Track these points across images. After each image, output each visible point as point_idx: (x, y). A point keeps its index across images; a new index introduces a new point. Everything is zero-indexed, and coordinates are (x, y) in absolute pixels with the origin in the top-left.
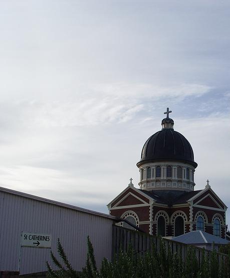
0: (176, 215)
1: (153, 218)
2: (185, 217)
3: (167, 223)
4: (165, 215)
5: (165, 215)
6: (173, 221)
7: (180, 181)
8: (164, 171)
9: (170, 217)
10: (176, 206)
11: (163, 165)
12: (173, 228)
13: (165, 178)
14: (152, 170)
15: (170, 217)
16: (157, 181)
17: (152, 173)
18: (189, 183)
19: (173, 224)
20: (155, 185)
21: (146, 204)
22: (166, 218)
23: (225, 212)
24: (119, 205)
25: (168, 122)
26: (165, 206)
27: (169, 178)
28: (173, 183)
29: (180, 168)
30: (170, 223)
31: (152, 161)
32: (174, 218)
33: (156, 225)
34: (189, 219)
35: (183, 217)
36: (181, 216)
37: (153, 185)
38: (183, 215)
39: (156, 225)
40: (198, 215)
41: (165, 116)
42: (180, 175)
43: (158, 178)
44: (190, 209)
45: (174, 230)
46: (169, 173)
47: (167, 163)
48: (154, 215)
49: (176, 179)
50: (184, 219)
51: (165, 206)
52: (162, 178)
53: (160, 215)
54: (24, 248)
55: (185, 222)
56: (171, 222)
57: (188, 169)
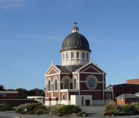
1: (61, 80)
16: (72, 60)
21: (58, 73)
29: (78, 54)
43: (72, 59)
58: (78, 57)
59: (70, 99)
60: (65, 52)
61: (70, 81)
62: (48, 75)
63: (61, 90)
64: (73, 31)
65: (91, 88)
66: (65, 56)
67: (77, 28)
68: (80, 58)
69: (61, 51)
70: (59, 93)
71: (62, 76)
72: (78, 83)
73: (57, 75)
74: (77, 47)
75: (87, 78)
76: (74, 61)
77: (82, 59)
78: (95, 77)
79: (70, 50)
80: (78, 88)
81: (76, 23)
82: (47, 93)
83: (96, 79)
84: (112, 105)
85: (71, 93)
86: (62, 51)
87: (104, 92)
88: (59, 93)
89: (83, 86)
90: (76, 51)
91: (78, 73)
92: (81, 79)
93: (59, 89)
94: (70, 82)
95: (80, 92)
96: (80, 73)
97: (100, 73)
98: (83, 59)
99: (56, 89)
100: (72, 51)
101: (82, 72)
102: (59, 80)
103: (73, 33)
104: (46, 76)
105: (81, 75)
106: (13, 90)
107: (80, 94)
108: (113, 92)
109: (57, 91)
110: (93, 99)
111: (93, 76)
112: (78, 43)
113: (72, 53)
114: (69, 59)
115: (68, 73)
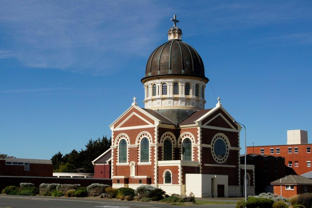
1: (159, 141)
2: (150, 138)
5: (171, 137)
6: (117, 143)
7: (176, 99)
11: (169, 83)
13: (171, 96)
14: (157, 87)
16: (163, 99)
20: (200, 104)
21: (151, 125)
23: (238, 133)
27: (176, 96)
29: (175, 85)
33: (162, 147)
39: (162, 147)
40: (165, 136)
47: (161, 80)
48: (159, 137)
49: (184, 96)
52: (168, 96)
54: (159, 181)
56: (179, 145)
58: (176, 91)
59: (184, 182)
60: (149, 83)
61: (174, 143)
62: (118, 129)
63: (160, 162)
64: (171, 37)
65: (219, 161)
66: (150, 90)
67: (180, 32)
68: (191, 96)
69: (145, 79)
70: (155, 167)
71: (161, 131)
72: (196, 148)
73: (151, 130)
74: (160, 72)
75: (213, 140)
77: (194, 97)
78: (226, 138)
79: (159, 79)
80: (196, 158)
81: (176, 21)
83: (228, 141)
84: (55, 170)
85: (187, 170)
86: (144, 80)
87: (239, 170)
88: (155, 167)
89: (205, 153)
90: (172, 80)
91: (199, 128)
92: (203, 141)
93: (156, 160)
94: (175, 145)
95: (201, 168)
96: (201, 128)
97: (234, 130)
99: (145, 157)
100: (188, 80)
101: (205, 126)
102: (154, 139)
103: (170, 41)
104: (112, 129)
105: (203, 131)
107: (201, 171)
108: (254, 170)
109: (150, 163)
110: (230, 184)
111: (223, 135)
112: (188, 63)
113: (163, 84)
114: (157, 96)
115: (172, 127)
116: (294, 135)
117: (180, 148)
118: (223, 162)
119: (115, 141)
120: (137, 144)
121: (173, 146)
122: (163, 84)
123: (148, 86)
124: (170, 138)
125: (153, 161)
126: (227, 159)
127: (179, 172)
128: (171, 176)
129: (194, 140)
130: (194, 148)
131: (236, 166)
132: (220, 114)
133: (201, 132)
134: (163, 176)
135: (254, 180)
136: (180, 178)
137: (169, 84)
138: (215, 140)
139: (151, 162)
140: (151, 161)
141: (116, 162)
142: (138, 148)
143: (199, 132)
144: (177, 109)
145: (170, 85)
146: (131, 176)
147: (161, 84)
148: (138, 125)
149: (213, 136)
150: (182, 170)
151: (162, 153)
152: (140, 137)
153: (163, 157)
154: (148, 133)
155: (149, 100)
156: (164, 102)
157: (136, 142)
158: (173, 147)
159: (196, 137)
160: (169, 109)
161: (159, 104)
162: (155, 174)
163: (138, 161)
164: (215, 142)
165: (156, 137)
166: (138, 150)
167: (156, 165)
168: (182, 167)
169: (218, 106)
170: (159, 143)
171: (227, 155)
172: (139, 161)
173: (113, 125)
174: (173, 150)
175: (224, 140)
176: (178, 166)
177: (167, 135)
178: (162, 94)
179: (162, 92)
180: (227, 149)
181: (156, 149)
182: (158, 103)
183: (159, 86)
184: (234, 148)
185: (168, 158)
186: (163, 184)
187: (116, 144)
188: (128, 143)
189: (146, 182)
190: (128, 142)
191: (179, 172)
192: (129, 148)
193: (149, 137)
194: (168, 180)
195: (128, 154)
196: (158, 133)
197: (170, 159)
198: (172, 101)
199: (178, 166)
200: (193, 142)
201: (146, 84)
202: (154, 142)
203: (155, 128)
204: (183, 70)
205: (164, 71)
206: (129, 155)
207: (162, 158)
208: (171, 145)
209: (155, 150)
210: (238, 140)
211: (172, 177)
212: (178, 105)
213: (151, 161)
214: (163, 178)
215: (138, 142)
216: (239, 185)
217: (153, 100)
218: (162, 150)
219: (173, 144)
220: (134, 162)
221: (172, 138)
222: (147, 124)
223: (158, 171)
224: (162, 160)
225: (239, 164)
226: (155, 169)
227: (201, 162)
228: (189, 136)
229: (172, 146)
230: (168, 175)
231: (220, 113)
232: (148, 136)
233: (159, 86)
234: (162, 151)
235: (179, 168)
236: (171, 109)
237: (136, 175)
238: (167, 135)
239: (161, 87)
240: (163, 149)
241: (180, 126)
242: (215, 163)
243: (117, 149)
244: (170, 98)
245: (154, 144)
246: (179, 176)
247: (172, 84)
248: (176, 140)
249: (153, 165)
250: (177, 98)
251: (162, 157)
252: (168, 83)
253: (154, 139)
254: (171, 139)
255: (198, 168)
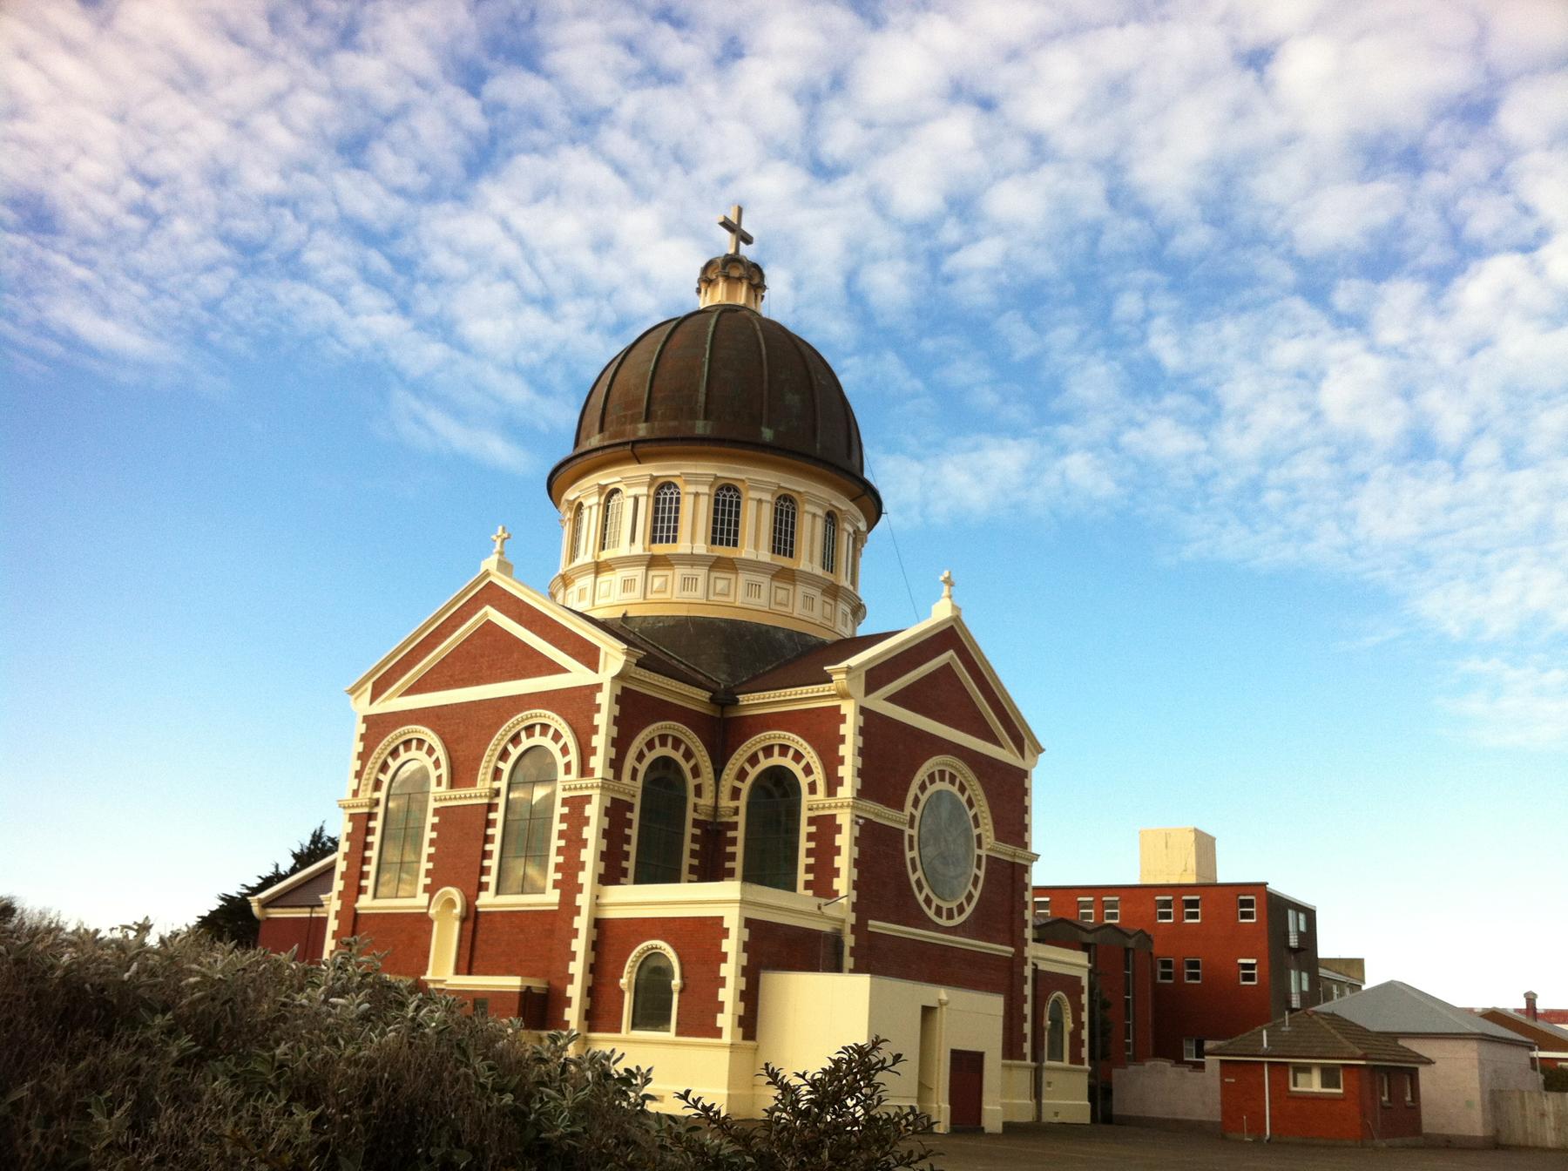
0: (753, 760)
1: (616, 764)
3: (697, 806)
4: (688, 755)
5: (688, 755)
6: (735, 793)
7: (786, 576)
8: (695, 514)
9: (718, 773)
10: (755, 702)
12: (733, 841)
13: (701, 548)
15: (718, 773)
16: (653, 562)
17: (845, 559)
18: (833, 592)
19: (737, 811)
21: (577, 675)
22: (696, 772)
24: (415, 689)
25: (1260, 79)
26: (696, 698)
28: (801, 589)
30: (716, 808)
31: (636, 452)
32: (742, 775)
33: (630, 807)
34: (833, 783)
35: (797, 769)
36: (787, 762)
37: (688, 583)
38: (802, 757)
40: (923, 788)
41: (725, 243)
42: (783, 540)
43: (661, 549)
44: (843, 719)
45: (739, 849)
46: (724, 526)
48: (620, 744)
49: (765, 555)
50: (804, 782)
51: (696, 698)
52: (683, 547)
53: (659, 751)
55: (812, 802)
57: (831, 518)
59: (749, 1024)
70: (581, 923)
72: (826, 827)
73: (576, 704)
74: (777, 435)
75: (914, 789)
76: (680, 572)
79: (638, 459)
82: (353, 921)
87: (1028, 971)
88: (581, 923)
91: (849, 708)
93: (586, 877)
95: (849, 941)
96: (863, 711)
97: (1004, 754)
98: (784, 561)
102: (586, 751)
106: (277, 877)
108: (1085, 982)
109: (550, 898)
116: (1166, 847)
117: (734, 826)
118: (958, 920)
119: (367, 770)
120: (484, 784)
121: (695, 811)
122: (662, 486)
123: (580, 505)
124: (682, 762)
125: (569, 887)
126: (973, 904)
127: (723, 957)
128: (676, 982)
129: (819, 776)
130: (811, 821)
131: (1012, 950)
132: (949, 656)
133: (862, 731)
134: (623, 982)
135: (1085, 1034)
136: (728, 995)
137: (692, 489)
138: (922, 792)
139: (558, 892)
140: (556, 884)
141: (361, 890)
142: (491, 807)
143: (849, 729)
144: (726, 621)
145: (697, 495)
146: (429, 976)
147: (650, 486)
148: (543, 911)
149: (914, 771)
150: (747, 947)
151: (628, 840)
152: (510, 747)
153: (630, 865)
154: (557, 722)
155: (582, 570)
156: (658, 578)
157: (480, 777)
158: (690, 815)
159: (832, 763)
160: (685, 614)
161: (632, 589)
162: (577, 968)
163: (482, 887)
164: (923, 799)
165: (600, 741)
166: (490, 823)
167: (585, 912)
168: (749, 923)
169: (941, 612)
170: (618, 776)
171: (975, 884)
172: (487, 890)
173: (369, 685)
174: (689, 830)
175: (963, 799)
176: (721, 918)
177: (663, 740)
178: (653, 540)
179: (654, 530)
180: (977, 851)
181: (593, 811)
182: (627, 585)
183: (636, 499)
184: (1005, 851)
185: (658, 869)
186: (618, 1030)
187: (370, 787)
188: (439, 783)
189: (466, 971)
190: (439, 778)
191: (723, 957)
192: (437, 812)
193: (561, 743)
194: (651, 1014)
195: (432, 842)
196: (617, 721)
197: (669, 875)
198: (701, 573)
199: (721, 918)
200: (813, 788)
201: (572, 498)
202: (585, 771)
203: (598, 687)
204: (769, 426)
205: (672, 424)
206: (432, 850)
207: (624, 873)
208: (684, 799)
209: (586, 821)
210: (1025, 810)
211: (682, 991)
212: (731, 599)
213: (556, 884)
214: (622, 993)
215: (497, 774)
216: (1023, 1057)
217: (599, 568)
218: (629, 823)
219: (691, 798)
220: (455, 893)
221: (692, 763)
222: (555, 669)
223: (596, 946)
224: (623, 880)
225: (1025, 943)
226: (573, 956)
227: (856, 907)
228: (791, 753)
229: (690, 806)
230: (653, 982)
231: (951, 652)
232: (557, 737)
233: (636, 499)
234: (627, 831)
235: (725, 933)
236: (692, 614)
237: (458, 971)
238: (663, 740)
239: (651, 500)
240: (635, 816)
241: (740, 697)
242: (922, 921)
243: (371, 816)
244: (691, 560)
245: (586, 781)
246: (722, 982)
247: (705, 489)
248: (711, 776)
249: (568, 908)
250: (731, 560)
251: (625, 864)
252: (687, 482)
253: (586, 751)
254: (686, 767)
255: (836, 940)
